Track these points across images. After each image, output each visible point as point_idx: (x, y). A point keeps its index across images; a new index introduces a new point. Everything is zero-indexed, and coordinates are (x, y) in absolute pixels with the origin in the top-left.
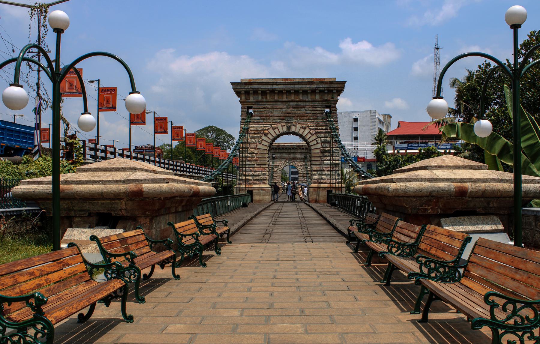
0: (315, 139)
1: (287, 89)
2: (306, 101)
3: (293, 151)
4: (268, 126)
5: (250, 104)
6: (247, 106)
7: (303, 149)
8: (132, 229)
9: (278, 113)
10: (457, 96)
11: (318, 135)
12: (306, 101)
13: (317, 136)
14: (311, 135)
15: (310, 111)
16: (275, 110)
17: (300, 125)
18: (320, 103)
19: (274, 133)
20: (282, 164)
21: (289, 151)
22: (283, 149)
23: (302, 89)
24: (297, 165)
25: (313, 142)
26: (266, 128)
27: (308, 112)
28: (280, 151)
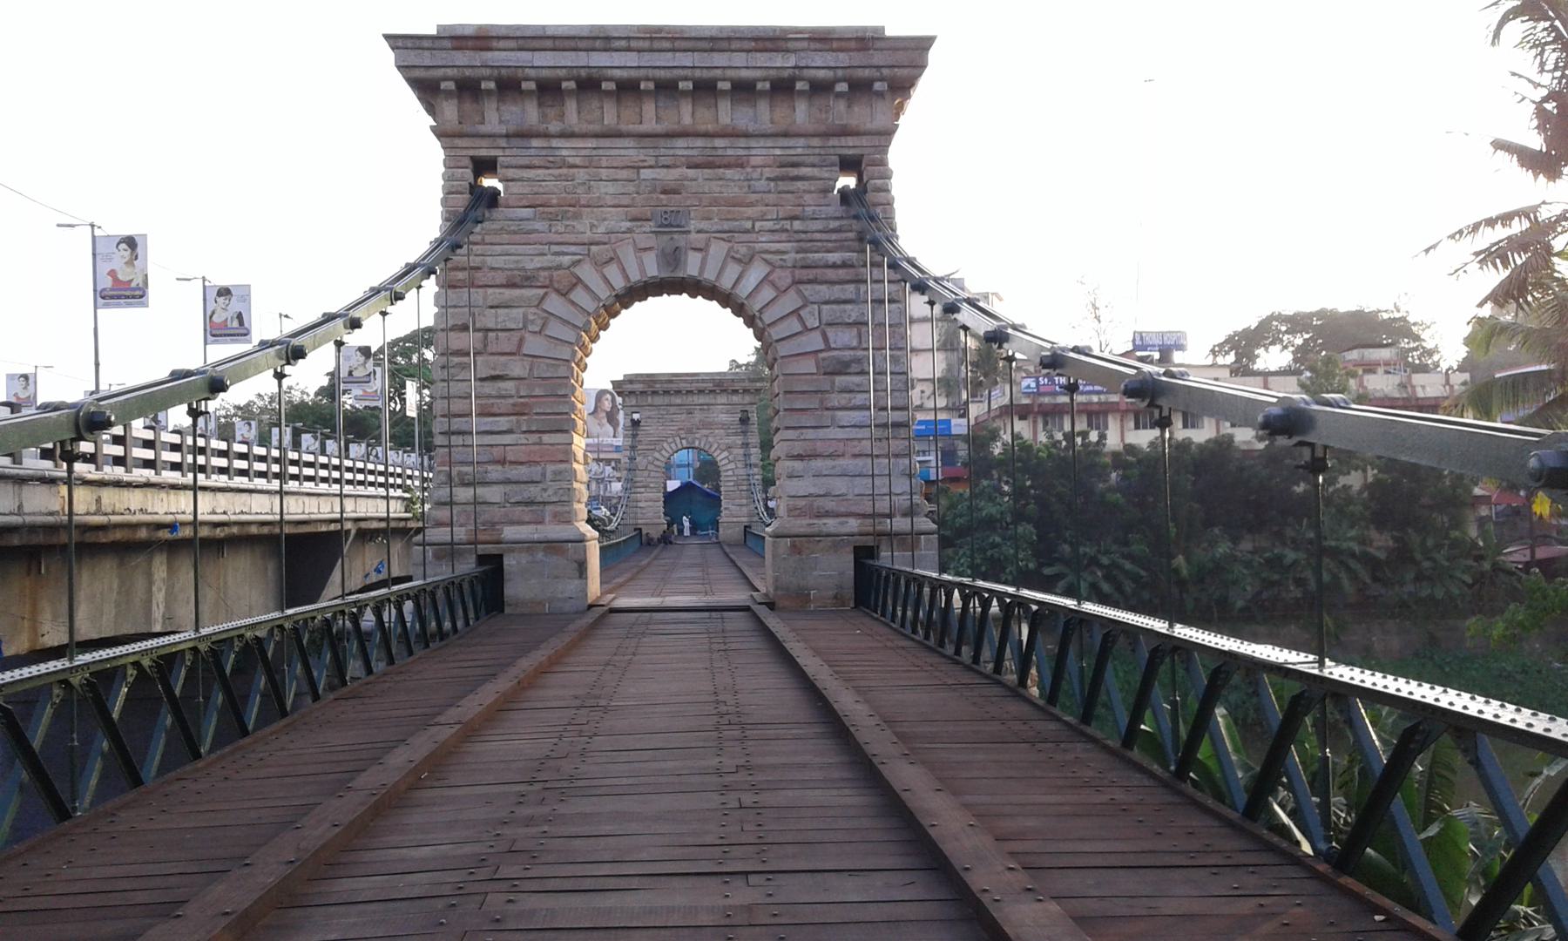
0: (796, 312)
3: (702, 399)
5: (484, 143)
6: (472, 153)
7: (735, 392)
11: (808, 290)
16: (604, 173)
20: (665, 445)
21: (690, 399)
22: (666, 393)
24: (716, 446)
25: (785, 323)
26: (566, 260)
27: (761, 185)
28: (658, 400)
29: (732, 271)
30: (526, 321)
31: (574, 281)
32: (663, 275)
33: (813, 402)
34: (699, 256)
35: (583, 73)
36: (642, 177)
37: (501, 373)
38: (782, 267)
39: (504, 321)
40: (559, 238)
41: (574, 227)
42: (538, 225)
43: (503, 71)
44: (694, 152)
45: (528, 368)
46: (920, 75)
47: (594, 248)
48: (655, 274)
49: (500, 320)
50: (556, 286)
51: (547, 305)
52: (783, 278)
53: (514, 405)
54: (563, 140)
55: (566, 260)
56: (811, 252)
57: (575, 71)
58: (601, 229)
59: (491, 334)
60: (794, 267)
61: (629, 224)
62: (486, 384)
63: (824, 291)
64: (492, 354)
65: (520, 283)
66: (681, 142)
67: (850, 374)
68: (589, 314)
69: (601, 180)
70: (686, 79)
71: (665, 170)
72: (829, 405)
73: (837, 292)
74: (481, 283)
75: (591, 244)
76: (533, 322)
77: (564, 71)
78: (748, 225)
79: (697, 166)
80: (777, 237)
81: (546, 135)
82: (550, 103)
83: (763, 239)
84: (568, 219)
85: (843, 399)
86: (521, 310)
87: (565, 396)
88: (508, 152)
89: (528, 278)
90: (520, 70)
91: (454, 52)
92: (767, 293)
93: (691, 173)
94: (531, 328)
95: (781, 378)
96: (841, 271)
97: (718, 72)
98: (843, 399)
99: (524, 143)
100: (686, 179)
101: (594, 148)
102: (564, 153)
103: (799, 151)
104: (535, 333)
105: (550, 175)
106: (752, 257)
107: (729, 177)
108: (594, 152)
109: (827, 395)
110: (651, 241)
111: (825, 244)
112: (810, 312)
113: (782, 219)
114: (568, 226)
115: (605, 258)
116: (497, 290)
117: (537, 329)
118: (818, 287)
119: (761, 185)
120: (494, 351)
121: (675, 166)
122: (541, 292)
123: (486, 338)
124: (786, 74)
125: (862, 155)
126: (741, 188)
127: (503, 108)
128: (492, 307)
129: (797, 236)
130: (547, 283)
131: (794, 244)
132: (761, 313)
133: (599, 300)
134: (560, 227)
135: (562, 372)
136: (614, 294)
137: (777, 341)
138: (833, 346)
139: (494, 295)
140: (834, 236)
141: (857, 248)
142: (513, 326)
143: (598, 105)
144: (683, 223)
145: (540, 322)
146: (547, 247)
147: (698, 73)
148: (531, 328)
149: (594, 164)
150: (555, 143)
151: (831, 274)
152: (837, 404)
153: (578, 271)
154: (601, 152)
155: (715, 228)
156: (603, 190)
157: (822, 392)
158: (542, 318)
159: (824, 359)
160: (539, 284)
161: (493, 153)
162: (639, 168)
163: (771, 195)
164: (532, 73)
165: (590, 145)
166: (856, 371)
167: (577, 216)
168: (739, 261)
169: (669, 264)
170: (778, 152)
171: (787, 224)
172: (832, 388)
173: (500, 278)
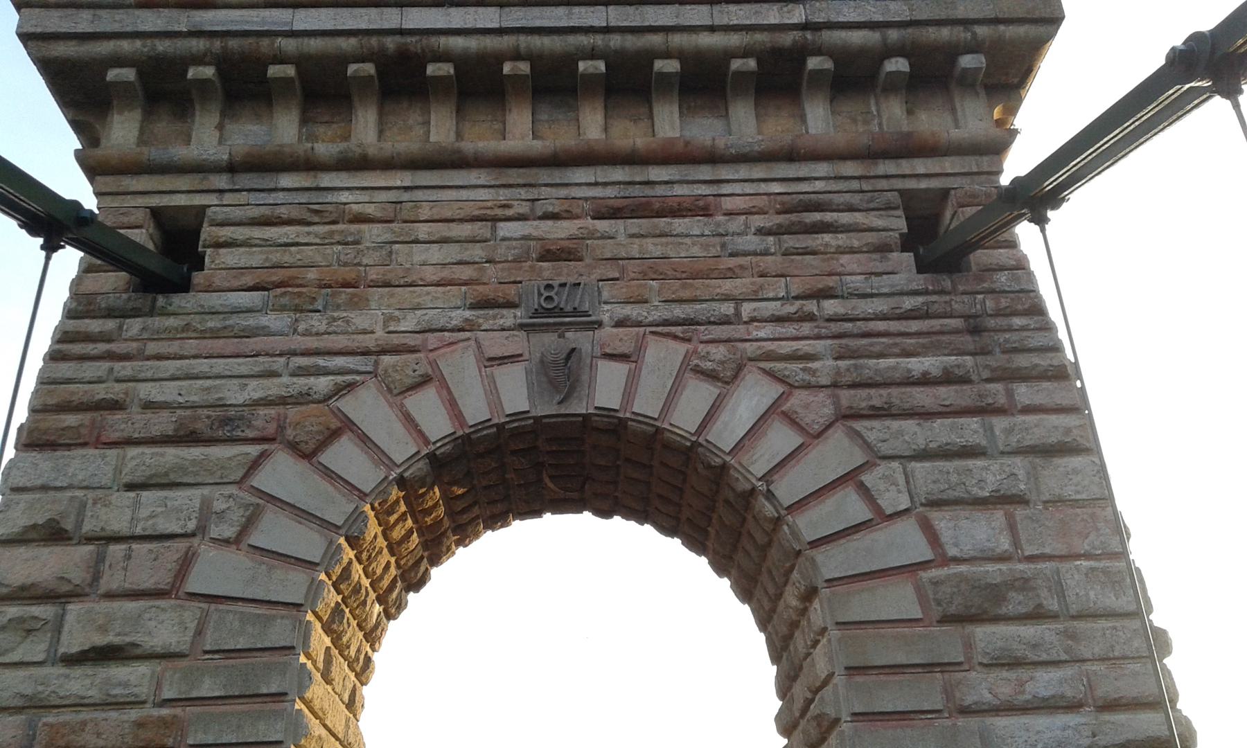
0: (850, 477)
1: (537, 42)
2: (713, 158)
4: (340, 361)
5: (183, 182)
6: (155, 201)
8: (1011, 251)
9: (452, 252)
10: (462, 542)
11: (873, 430)
12: (713, 158)
13: (867, 446)
14: (795, 440)
15: (761, 232)
16: (423, 231)
17: (682, 348)
18: (850, 168)
19: (399, 428)
23: (677, 40)
25: (829, 504)
26: (323, 384)
27: (751, 242)
29: (697, 396)
30: (206, 514)
31: (335, 423)
32: (539, 411)
33: (929, 695)
34: (621, 369)
35: (391, 43)
36: (501, 233)
37: (117, 640)
38: (807, 386)
39: (151, 517)
40: (312, 343)
41: (348, 322)
42: (272, 320)
43: (233, 43)
44: (610, 192)
45: (192, 626)
46: (1050, 36)
47: (387, 359)
48: (523, 406)
49: (144, 513)
50: (290, 433)
51: (262, 480)
52: (815, 408)
53: (140, 724)
54: (344, 175)
55: (323, 384)
56: (870, 357)
57: (374, 41)
58: (409, 323)
59: (116, 550)
60: (835, 385)
61: (468, 314)
62: (78, 671)
63: (913, 433)
64: (110, 596)
65: (208, 433)
66: (581, 175)
67: (1007, 619)
68: (363, 496)
69: (416, 241)
70: (592, 54)
71: (550, 223)
72: (969, 700)
73: (941, 432)
74: (115, 436)
75: (384, 352)
76: (221, 515)
77: (353, 41)
78: (727, 309)
79: (614, 213)
80: (790, 329)
81: (311, 165)
82: (326, 118)
83: (762, 334)
84: (338, 307)
85: (999, 685)
86: (197, 493)
87: (280, 696)
88: (229, 198)
89: (226, 421)
90: (265, 42)
91: (138, 12)
92: (781, 440)
93: (603, 225)
94: (215, 531)
95: (834, 633)
96: (943, 391)
97: (656, 40)
98: (999, 685)
99: (266, 181)
100: (592, 235)
101: (406, 189)
102: (344, 197)
103: (819, 185)
104: (227, 542)
105: (309, 233)
106: (739, 369)
107: (679, 230)
108: (406, 196)
109: (959, 675)
110: (516, 343)
111: (898, 340)
112: (884, 477)
113: (796, 298)
114: (335, 320)
115: (409, 379)
116: (148, 450)
117: (229, 532)
118: (895, 424)
119: (751, 242)
120: (114, 586)
121: (569, 215)
122: (254, 450)
123: (100, 559)
124: (787, 39)
125: (945, 193)
126: (706, 247)
127: (230, 127)
128: (130, 487)
129: (835, 328)
130: (271, 429)
131: (829, 342)
132: (769, 483)
133: (391, 464)
134: (317, 322)
135: (278, 634)
136: (425, 451)
137: (815, 544)
138: (952, 552)
139: (140, 460)
140: (914, 326)
141: (971, 347)
142: (174, 528)
143: (420, 119)
144: (586, 307)
145: (237, 516)
146: (282, 360)
147: (616, 41)
148: (215, 531)
149: (405, 215)
150: (327, 180)
151: (922, 397)
152: (988, 697)
153: (347, 405)
154: (419, 195)
155: (655, 316)
156: (418, 258)
157: (944, 667)
158: (247, 506)
159: (936, 583)
160: (250, 434)
161: (198, 200)
162: (495, 220)
163: (769, 258)
164: (289, 45)
165: (399, 183)
166: (1022, 610)
167: (358, 304)
168: (711, 376)
169: (554, 385)
170: (776, 188)
171: (811, 306)
172: (969, 659)
173: (163, 423)
